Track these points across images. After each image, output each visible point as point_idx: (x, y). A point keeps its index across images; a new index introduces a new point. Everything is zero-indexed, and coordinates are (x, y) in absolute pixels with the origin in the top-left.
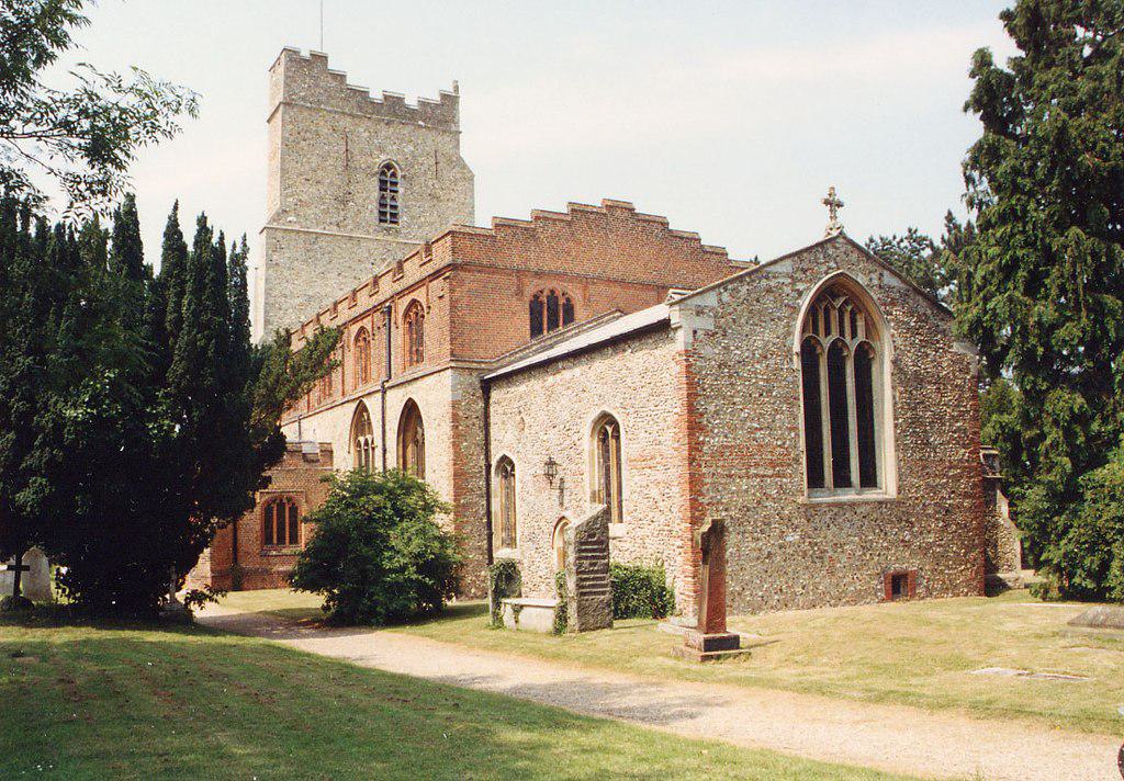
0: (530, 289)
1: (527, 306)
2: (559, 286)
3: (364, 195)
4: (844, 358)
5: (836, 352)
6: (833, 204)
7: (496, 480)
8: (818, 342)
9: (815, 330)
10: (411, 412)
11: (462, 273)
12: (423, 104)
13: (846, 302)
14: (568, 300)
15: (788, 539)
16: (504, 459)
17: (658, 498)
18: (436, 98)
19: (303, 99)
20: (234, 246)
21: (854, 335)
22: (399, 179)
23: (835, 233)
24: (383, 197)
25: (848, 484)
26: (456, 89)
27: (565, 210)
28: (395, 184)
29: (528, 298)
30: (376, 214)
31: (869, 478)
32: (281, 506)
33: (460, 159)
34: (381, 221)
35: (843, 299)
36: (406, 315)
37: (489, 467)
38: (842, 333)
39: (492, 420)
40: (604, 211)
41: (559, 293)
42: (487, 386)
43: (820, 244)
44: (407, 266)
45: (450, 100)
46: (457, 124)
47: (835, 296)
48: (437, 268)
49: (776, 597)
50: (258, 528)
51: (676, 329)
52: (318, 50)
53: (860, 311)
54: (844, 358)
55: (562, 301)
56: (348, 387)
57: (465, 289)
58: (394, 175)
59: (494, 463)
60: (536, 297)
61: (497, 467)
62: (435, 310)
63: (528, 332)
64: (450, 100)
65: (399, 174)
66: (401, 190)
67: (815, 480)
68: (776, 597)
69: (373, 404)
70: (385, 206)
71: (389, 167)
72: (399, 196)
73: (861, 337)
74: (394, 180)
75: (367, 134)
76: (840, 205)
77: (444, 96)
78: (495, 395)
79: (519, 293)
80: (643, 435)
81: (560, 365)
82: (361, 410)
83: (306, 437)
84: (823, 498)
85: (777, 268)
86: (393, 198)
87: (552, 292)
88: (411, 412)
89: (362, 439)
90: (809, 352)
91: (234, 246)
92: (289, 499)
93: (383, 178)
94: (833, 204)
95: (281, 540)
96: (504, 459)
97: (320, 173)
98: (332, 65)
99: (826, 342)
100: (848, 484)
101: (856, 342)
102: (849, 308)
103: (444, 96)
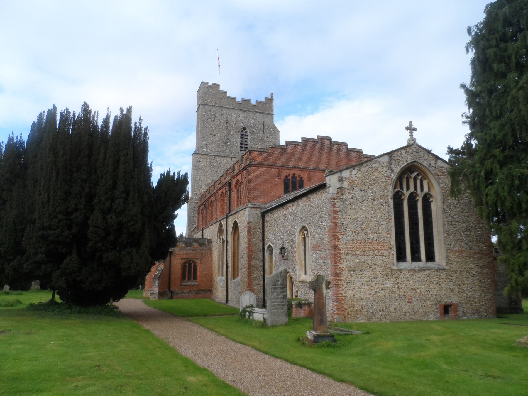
0: (284, 173)
1: (283, 181)
2: (297, 173)
3: (234, 140)
4: (403, 199)
5: (412, 199)
6: (411, 129)
7: (267, 254)
8: (403, 194)
9: (401, 188)
10: (236, 226)
11: (254, 168)
12: (258, 102)
13: (418, 175)
14: (301, 178)
15: (386, 285)
16: (269, 246)
17: (322, 264)
18: (263, 100)
19: (209, 102)
20: (17, 137)
21: (408, 188)
22: (248, 134)
23: (411, 142)
24: (242, 141)
25: (419, 260)
26: (272, 97)
27: (300, 141)
28: (247, 135)
29: (283, 177)
30: (239, 148)
31: (430, 257)
32: (190, 265)
33: (367, 156)
34: (241, 150)
35: (416, 174)
36: (236, 186)
37: (264, 249)
38: (416, 188)
39: (266, 229)
40: (318, 141)
41: (297, 175)
42: (263, 215)
43: (404, 148)
44: (236, 166)
45: (270, 101)
46: (272, 110)
47: (412, 172)
48: (245, 166)
49: (380, 313)
50: (180, 273)
51: (329, 187)
52: (216, 82)
53: (425, 179)
54: (403, 199)
55: (298, 179)
56: (218, 217)
57: (255, 174)
58: (246, 132)
59: (266, 248)
60: (286, 177)
61: (267, 249)
62: (244, 184)
63: (283, 192)
64: (270, 101)
65: (248, 132)
66: (249, 137)
67: (401, 257)
68: (380, 313)
69: (224, 222)
70: (243, 144)
71: (244, 129)
72: (248, 140)
73: (412, 189)
74: (246, 134)
75: (235, 116)
76: (415, 129)
77: (267, 99)
78: (267, 218)
79: (279, 176)
80: (317, 235)
81: (288, 205)
82: (221, 226)
83: (205, 236)
84: (403, 265)
85: (381, 159)
86: (246, 141)
87: (294, 174)
88: (236, 226)
89: (221, 237)
90: (397, 198)
91: (17, 137)
92: (193, 262)
93: (242, 133)
94: (411, 129)
95: (189, 279)
96: (269, 246)
97: (216, 131)
98: (221, 88)
99: (406, 194)
100: (419, 260)
101: (423, 193)
102: (420, 177)
103: (267, 99)
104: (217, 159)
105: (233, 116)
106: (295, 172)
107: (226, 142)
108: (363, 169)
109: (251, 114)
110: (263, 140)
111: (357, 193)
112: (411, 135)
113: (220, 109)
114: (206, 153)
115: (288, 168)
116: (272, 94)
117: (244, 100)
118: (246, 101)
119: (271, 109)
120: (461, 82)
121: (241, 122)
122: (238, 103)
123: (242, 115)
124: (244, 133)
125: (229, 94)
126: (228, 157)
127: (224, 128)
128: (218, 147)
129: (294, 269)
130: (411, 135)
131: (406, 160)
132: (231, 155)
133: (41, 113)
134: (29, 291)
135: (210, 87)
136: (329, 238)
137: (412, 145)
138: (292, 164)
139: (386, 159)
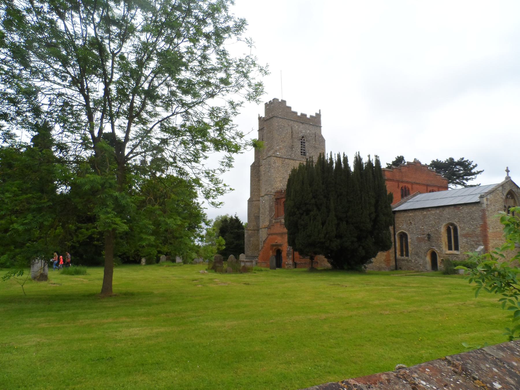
0: (401, 185)
6: (508, 171)
12: (311, 116)
18: (314, 115)
24: (301, 147)
30: (300, 153)
45: (318, 115)
52: (284, 99)
64: (318, 115)
71: (303, 137)
103: (317, 114)
104: (287, 161)
105: (296, 126)
106: (405, 184)
107: (292, 147)
108: (494, 194)
109: (307, 126)
110: (315, 147)
111: (493, 207)
112: (508, 175)
113: (287, 121)
114: (279, 156)
115: (402, 182)
116: (320, 110)
117: (302, 114)
118: (304, 116)
119: (319, 122)
120: (248, 22)
121: (301, 132)
122: (299, 117)
123: (302, 126)
124: (303, 141)
125: (293, 110)
126: (293, 160)
127: (290, 136)
128: (287, 151)
129: (439, 247)
130: (508, 175)
131: (508, 188)
132: (295, 158)
133: (356, 157)
134: (159, 264)
135: (280, 102)
136: (481, 230)
137: (509, 181)
138: (405, 179)
139: (501, 188)
